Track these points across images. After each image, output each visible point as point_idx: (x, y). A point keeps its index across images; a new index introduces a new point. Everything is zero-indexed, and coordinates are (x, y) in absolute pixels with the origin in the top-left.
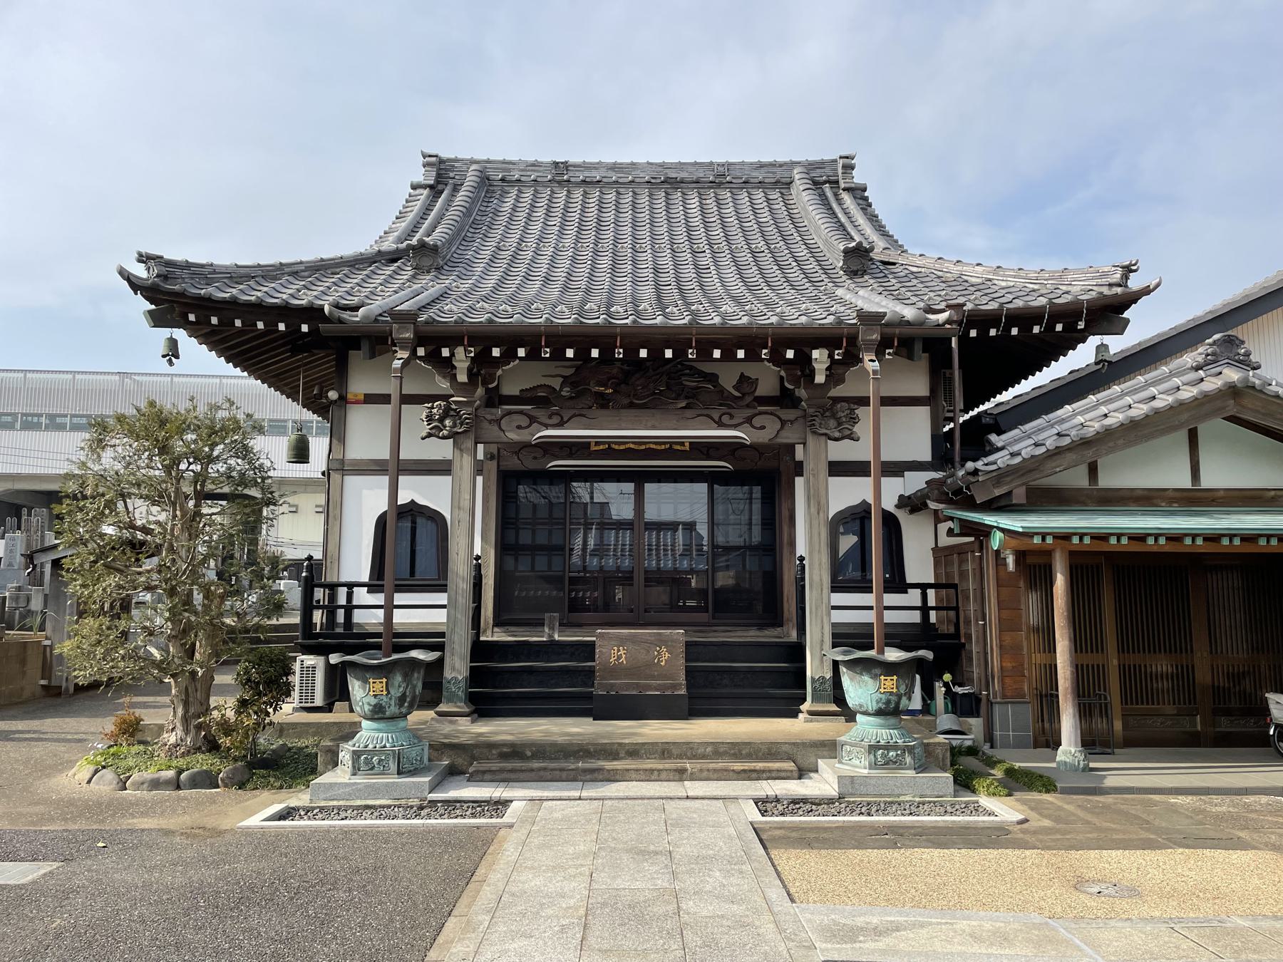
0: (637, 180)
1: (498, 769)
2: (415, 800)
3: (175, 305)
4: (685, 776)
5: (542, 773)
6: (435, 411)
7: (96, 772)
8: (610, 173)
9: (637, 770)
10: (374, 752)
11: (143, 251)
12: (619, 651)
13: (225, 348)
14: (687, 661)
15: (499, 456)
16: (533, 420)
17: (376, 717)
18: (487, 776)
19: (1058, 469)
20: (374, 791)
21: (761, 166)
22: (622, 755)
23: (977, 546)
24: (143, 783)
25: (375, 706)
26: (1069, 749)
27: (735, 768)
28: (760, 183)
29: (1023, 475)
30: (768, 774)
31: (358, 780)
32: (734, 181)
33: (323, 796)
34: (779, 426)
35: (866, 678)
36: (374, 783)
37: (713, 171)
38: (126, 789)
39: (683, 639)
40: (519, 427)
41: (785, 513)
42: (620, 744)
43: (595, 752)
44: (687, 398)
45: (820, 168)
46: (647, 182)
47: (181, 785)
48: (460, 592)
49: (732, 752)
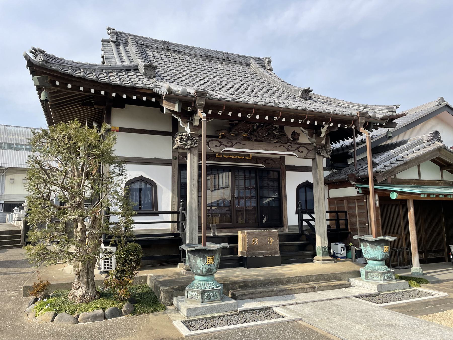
0: (197, 54)
1: (247, 293)
2: (232, 311)
3: (48, 76)
4: (315, 290)
5: (265, 293)
6: (184, 137)
7: (55, 315)
8: (186, 50)
9: (299, 289)
10: (209, 291)
11: (37, 48)
12: (255, 239)
13: (52, 101)
14: (279, 242)
15: (178, 158)
16: (221, 143)
17: (207, 274)
18: (244, 297)
19: (399, 172)
20: (214, 309)
21: (240, 56)
22: (284, 283)
23: (365, 197)
24: (88, 318)
25: (208, 269)
26: (416, 267)
27: (331, 284)
28: (240, 62)
29: (390, 173)
30: (342, 286)
31: (204, 305)
32: (231, 60)
33: (193, 314)
34: (307, 152)
35: (379, 247)
36: (215, 306)
37: (223, 55)
38: (78, 322)
39: (277, 234)
40: (216, 146)
41: (283, 184)
42: (284, 278)
43: (275, 282)
44: (277, 139)
45: (259, 60)
46: (200, 55)
47: (107, 317)
48: (195, 215)
49: (322, 278)
